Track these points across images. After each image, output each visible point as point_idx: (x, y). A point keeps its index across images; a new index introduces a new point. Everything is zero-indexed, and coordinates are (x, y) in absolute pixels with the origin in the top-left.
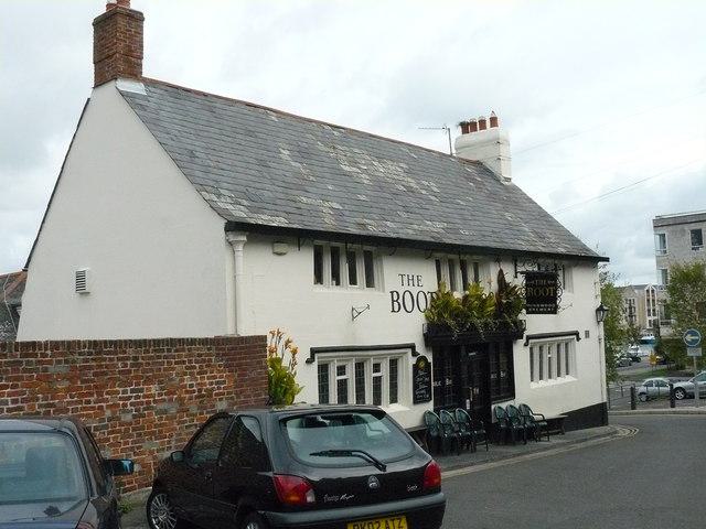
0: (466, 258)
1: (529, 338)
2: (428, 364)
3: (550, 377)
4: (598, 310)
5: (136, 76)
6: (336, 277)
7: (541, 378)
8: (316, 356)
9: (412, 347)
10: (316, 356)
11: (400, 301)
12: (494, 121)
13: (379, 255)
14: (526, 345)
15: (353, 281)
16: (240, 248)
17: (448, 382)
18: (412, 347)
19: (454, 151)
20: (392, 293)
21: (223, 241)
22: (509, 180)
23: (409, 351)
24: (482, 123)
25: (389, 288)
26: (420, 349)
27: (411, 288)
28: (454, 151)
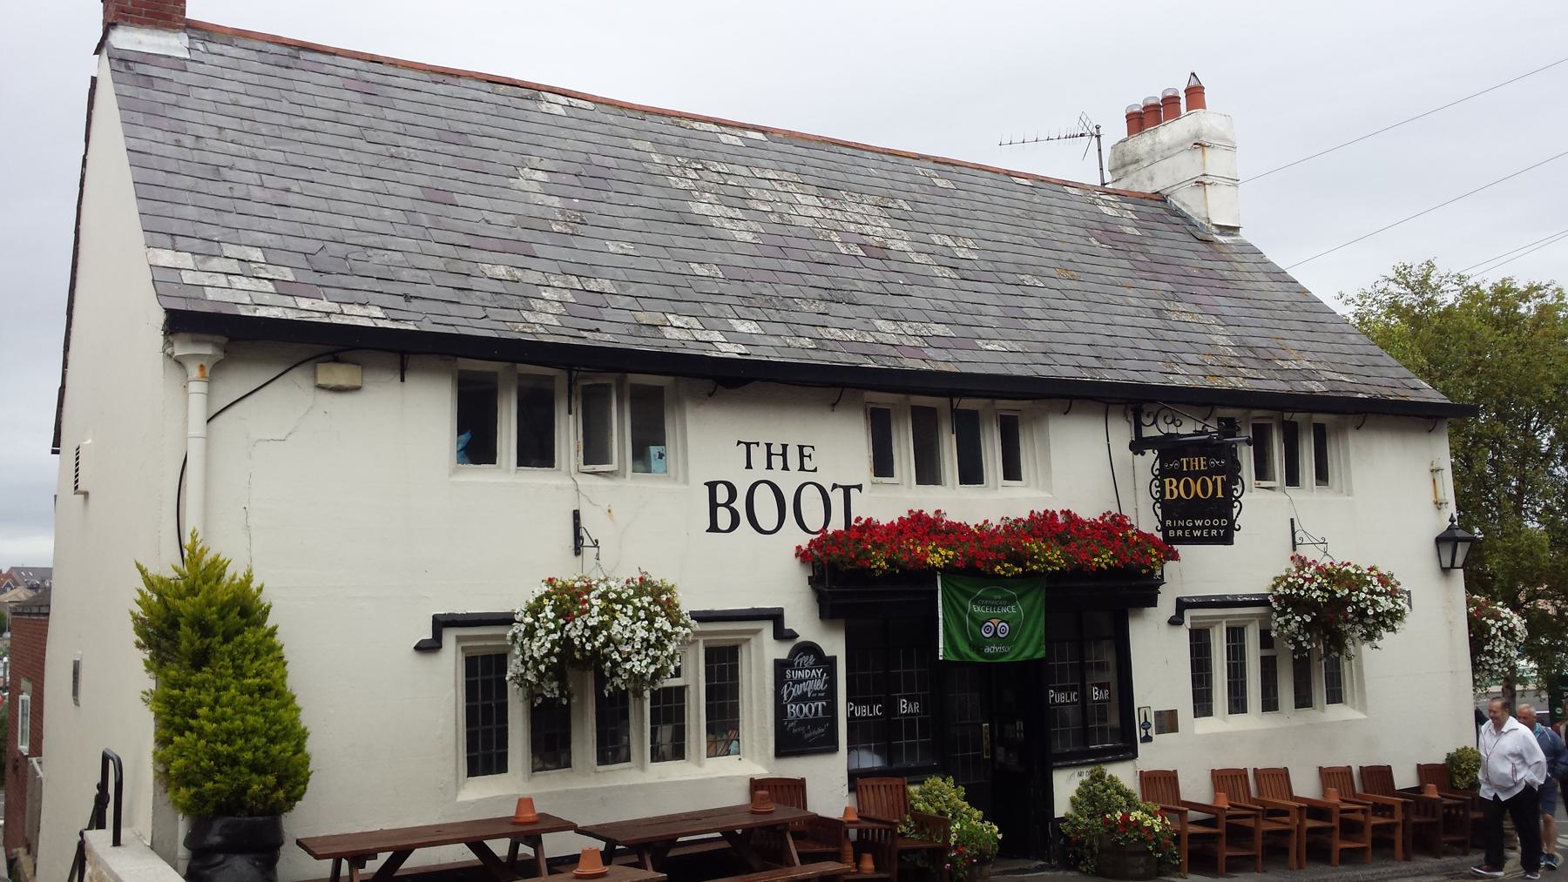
0: (1298, 417)
1: (1182, 605)
2: (829, 664)
3: (1238, 704)
4: (1439, 541)
5: (168, 17)
6: (595, 452)
7: (1238, 704)
8: (1188, 614)
9: (776, 617)
10: (1188, 614)
11: (740, 505)
12: (1195, 94)
13: (679, 402)
14: (1176, 621)
15: (1292, 479)
16: (194, 371)
17: (904, 707)
18: (776, 617)
19: (1108, 177)
20: (712, 486)
21: (159, 358)
22: (1232, 230)
23: (767, 628)
24: (1170, 102)
25: (703, 473)
26: (803, 621)
27: (776, 476)
28: (1108, 177)
